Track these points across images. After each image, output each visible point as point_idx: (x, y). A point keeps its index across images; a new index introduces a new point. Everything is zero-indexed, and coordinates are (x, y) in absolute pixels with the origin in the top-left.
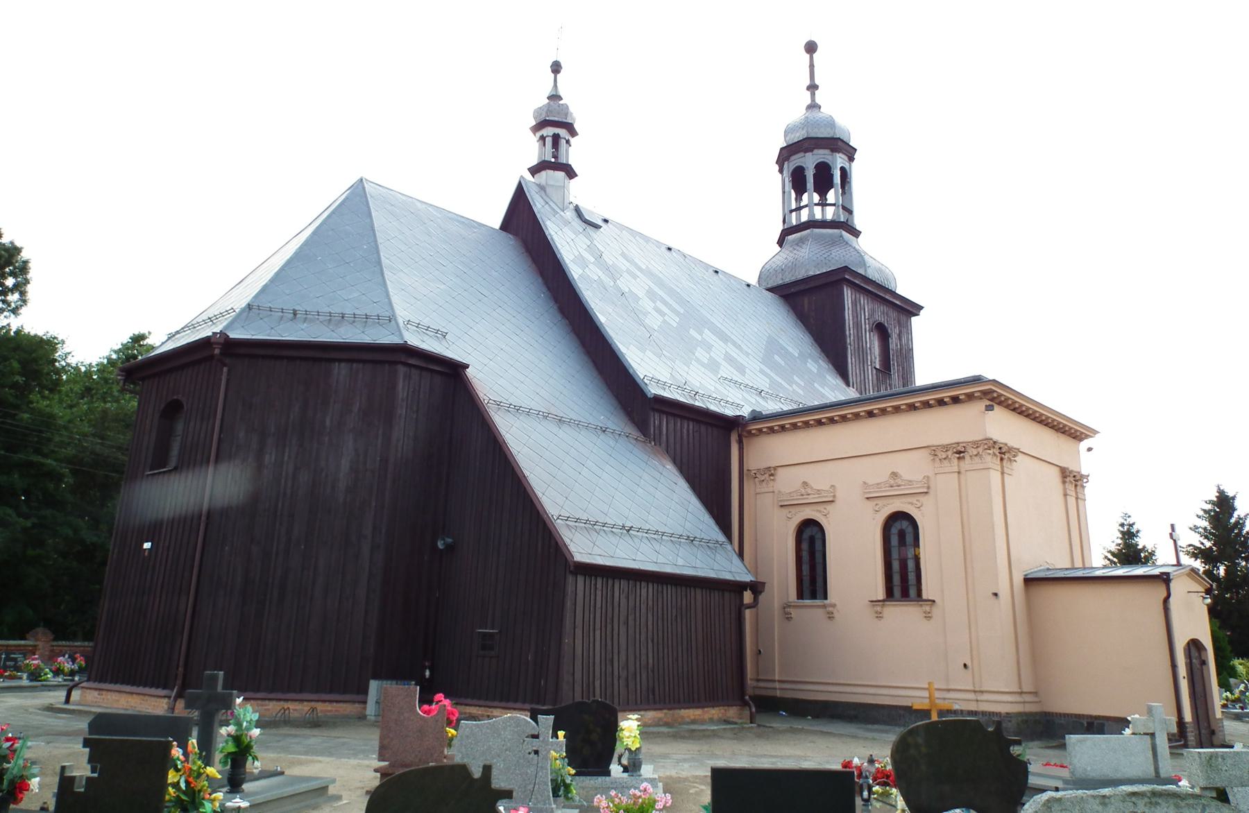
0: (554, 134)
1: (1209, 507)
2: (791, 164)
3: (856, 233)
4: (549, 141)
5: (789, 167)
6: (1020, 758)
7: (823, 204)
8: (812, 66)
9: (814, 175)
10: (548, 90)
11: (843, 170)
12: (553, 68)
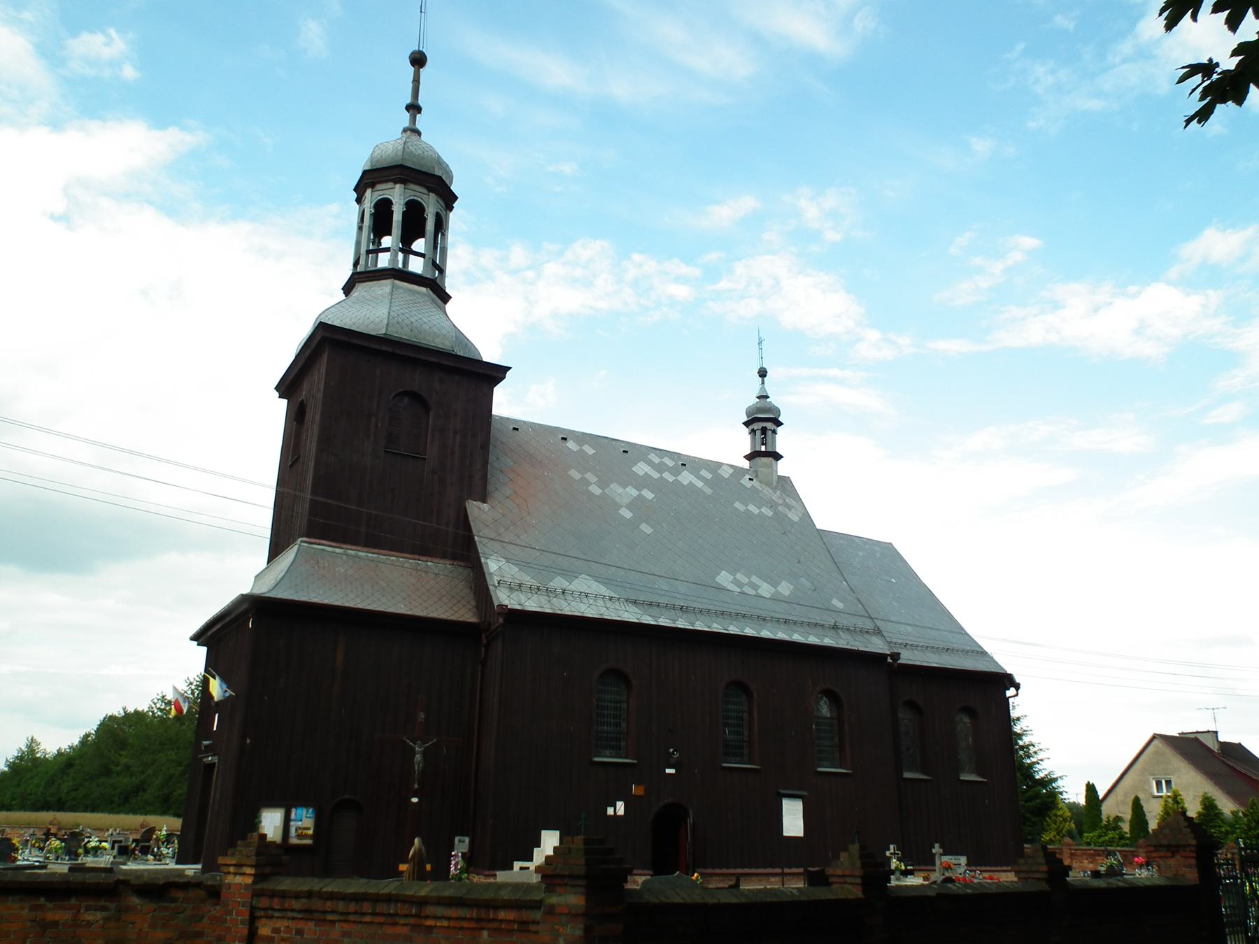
1: (1041, 755)
2: (376, 194)
3: (445, 298)
4: (758, 433)
5: (370, 198)
7: (407, 251)
9: (404, 213)
10: (756, 391)
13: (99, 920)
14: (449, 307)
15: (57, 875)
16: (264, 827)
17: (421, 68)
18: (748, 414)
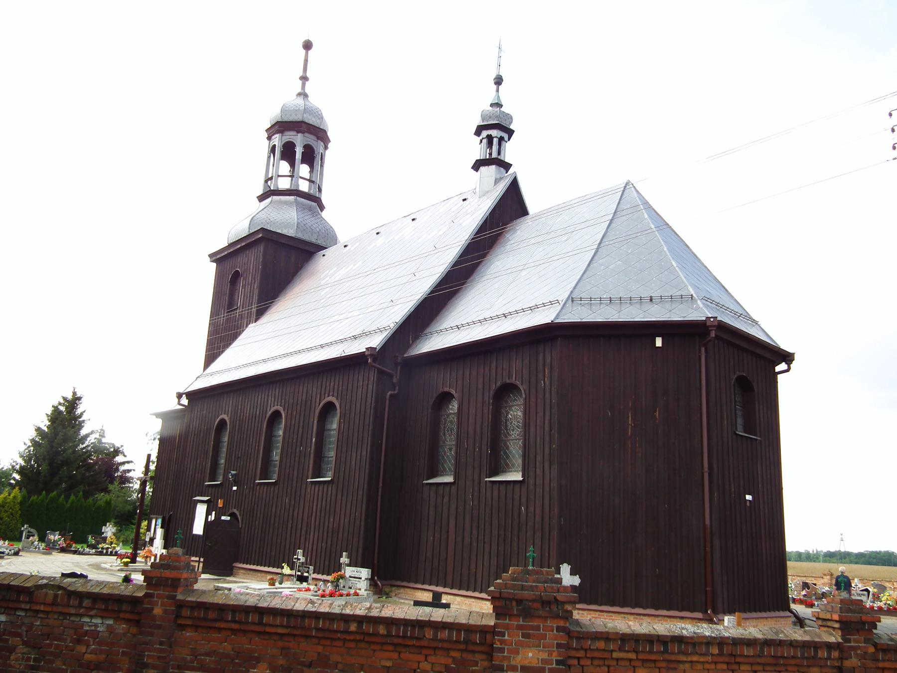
0: (488, 135)
3: (322, 208)
4: (485, 141)
5: (277, 140)
6: (269, 606)
8: (306, 61)
10: (491, 99)
11: (322, 153)
12: (495, 80)
13: (97, 609)
14: (324, 214)
15: (301, 612)
16: (161, 539)
17: (309, 50)
18: (483, 118)
